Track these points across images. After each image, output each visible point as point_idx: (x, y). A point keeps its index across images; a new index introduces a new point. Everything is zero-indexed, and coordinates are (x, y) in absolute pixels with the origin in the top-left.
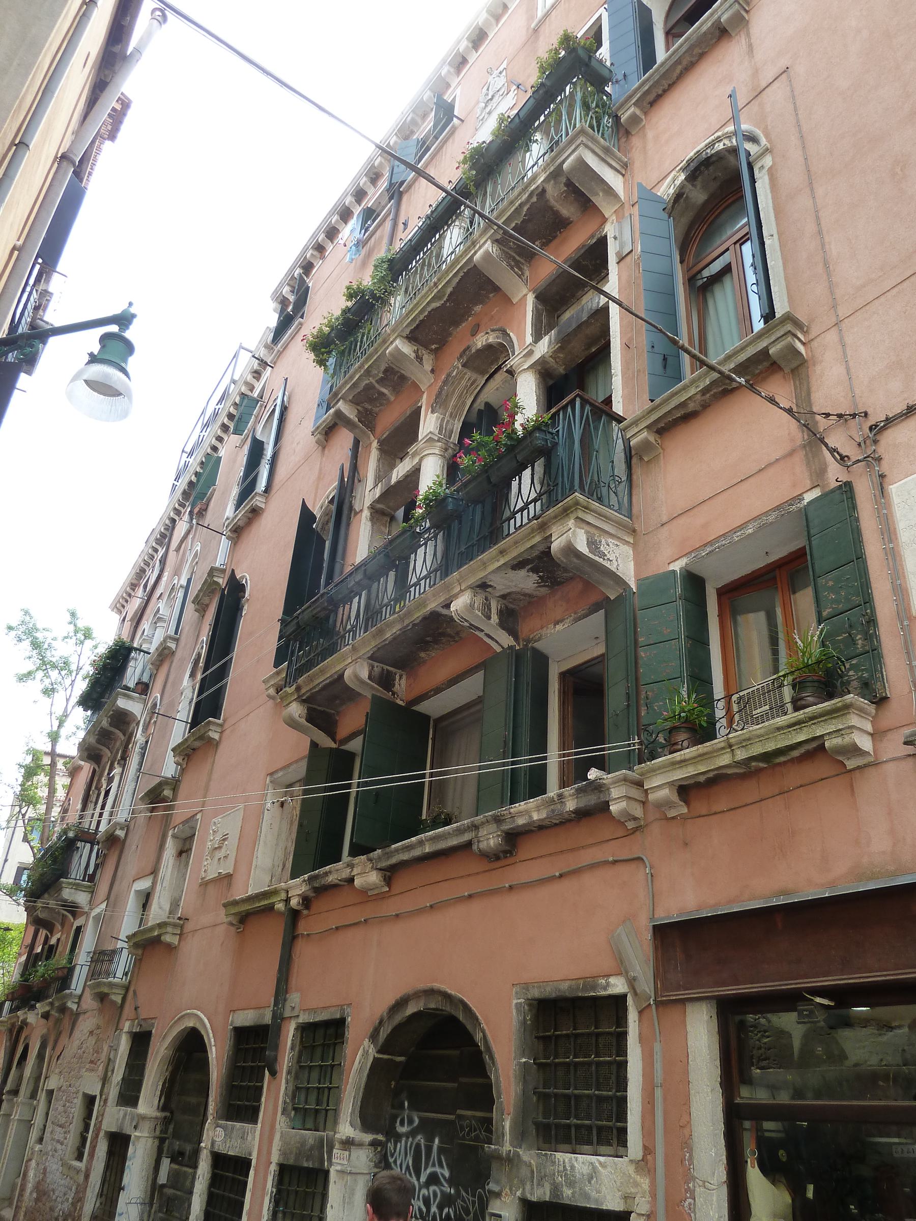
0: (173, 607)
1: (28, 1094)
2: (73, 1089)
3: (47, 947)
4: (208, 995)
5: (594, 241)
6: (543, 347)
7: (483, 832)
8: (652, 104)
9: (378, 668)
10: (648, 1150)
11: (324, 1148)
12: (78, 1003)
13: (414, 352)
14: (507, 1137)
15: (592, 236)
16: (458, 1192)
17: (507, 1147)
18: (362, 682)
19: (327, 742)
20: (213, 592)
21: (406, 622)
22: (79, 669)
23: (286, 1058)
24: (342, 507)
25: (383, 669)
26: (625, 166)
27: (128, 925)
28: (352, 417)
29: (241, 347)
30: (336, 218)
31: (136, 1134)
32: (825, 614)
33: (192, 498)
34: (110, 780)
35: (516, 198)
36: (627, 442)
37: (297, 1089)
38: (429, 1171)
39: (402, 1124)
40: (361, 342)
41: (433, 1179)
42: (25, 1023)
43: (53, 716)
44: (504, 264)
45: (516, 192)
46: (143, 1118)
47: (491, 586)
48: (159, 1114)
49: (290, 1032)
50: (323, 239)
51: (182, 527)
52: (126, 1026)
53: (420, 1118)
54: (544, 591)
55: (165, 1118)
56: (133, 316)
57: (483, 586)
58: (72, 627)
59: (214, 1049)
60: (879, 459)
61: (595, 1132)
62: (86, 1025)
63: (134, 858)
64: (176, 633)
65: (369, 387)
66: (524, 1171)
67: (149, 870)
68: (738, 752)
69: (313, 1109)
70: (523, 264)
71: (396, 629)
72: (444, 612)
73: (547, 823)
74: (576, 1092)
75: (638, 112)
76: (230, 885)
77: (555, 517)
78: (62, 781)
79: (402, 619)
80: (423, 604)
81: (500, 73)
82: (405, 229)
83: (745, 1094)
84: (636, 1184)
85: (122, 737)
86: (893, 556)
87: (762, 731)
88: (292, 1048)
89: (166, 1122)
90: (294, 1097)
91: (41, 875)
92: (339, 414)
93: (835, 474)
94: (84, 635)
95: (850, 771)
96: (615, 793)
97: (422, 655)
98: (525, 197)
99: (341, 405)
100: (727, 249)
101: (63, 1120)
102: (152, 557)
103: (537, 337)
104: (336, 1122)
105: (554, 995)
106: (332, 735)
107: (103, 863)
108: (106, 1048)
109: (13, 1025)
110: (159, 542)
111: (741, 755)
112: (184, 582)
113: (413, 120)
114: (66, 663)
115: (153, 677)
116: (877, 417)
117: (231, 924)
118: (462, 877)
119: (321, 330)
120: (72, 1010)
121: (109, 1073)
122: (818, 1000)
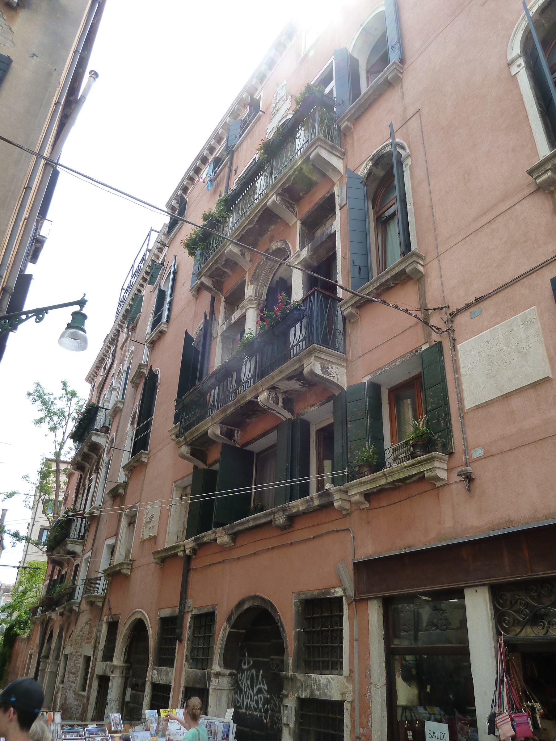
0: (120, 382)
1: (54, 658)
2: (78, 654)
3: (60, 576)
4: (147, 601)
5: (329, 195)
6: (305, 253)
7: (277, 516)
8: (356, 119)
9: (225, 428)
10: (351, 671)
11: (206, 678)
12: (79, 607)
13: (240, 251)
14: (291, 668)
15: (328, 192)
16: (271, 696)
17: (291, 673)
18: (217, 436)
19: (202, 466)
20: (141, 376)
21: (237, 406)
22: (70, 415)
23: (187, 633)
24: (207, 333)
25: (228, 428)
26: (343, 154)
27: (104, 565)
28: (209, 285)
29: (152, 230)
30: (199, 162)
31: (113, 675)
32: (428, 409)
33: (128, 319)
34: (90, 481)
35: (287, 172)
36: (342, 312)
37: (193, 649)
38: (258, 687)
39: (245, 664)
40: (213, 244)
41: (260, 691)
42: (50, 619)
43: (57, 443)
44: (283, 206)
45: (288, 168)
46: (116, 667)
47: (277, 388)
48: (124, 665)
49: (188, 619)
50: (193, 174)
51: (123, 337)
52: (105, 619)
53: (254, 662)
54: (305, 389)
55: (127, 666)
56: (86, 301)
57: (273, 388)
58: (64, 392)
59: (151, 629)
60: (453, 331)
61: (330, 664)
62: (83, 618)
63: (105, 528)
64: (122, 399)
65: (218, 269)
66: (298, 684)
67: (113, 534)
68: (388, 478)
69: (201, 658)
70: (294, 205)
71: (232, 409)
72: (256, 400)
73: (306, 511)
74: (322, 645)
75: (349, 124)
76: (155, 542)
77: (305, 355)
78: (63, 478)
79: (234, 404)
80: (245, 397)
81: (283, 87)
82: (236, 173)
83: (396, 642)
84: (347, 688)
85: (96, 457)
86: (458, 381)
87: (398, 468)
88: (190, 628)
89: (128, 669)
90: (191, 653)
91: (55, 536)
92: (202, 284)
93: (435, 338)
94: (71, 395)
95: (438, 487)
96: (336, 497)
97: (248, 420)
98: (291, 172)
99: (203, 279)
100: (394, 204)
101: (74, 670)
102: (108, 352)
103: (301, 249)
104: (212, 665)
105: (311, 597)
106: (205, 462)
107: (89, 529)
108: (95, 631)
109: (44, 620)
110: (111, 343)
111: (390, 480)
112: (125, 368)
113: (238, 109)
114: (62, 412)
115: (111, 423)
116: (453, 309)
117: (157, 563)
118: (269, 538)
119: (191, 236)
120: (76, 611)
121: (97, 644)
122: (423, 598)
